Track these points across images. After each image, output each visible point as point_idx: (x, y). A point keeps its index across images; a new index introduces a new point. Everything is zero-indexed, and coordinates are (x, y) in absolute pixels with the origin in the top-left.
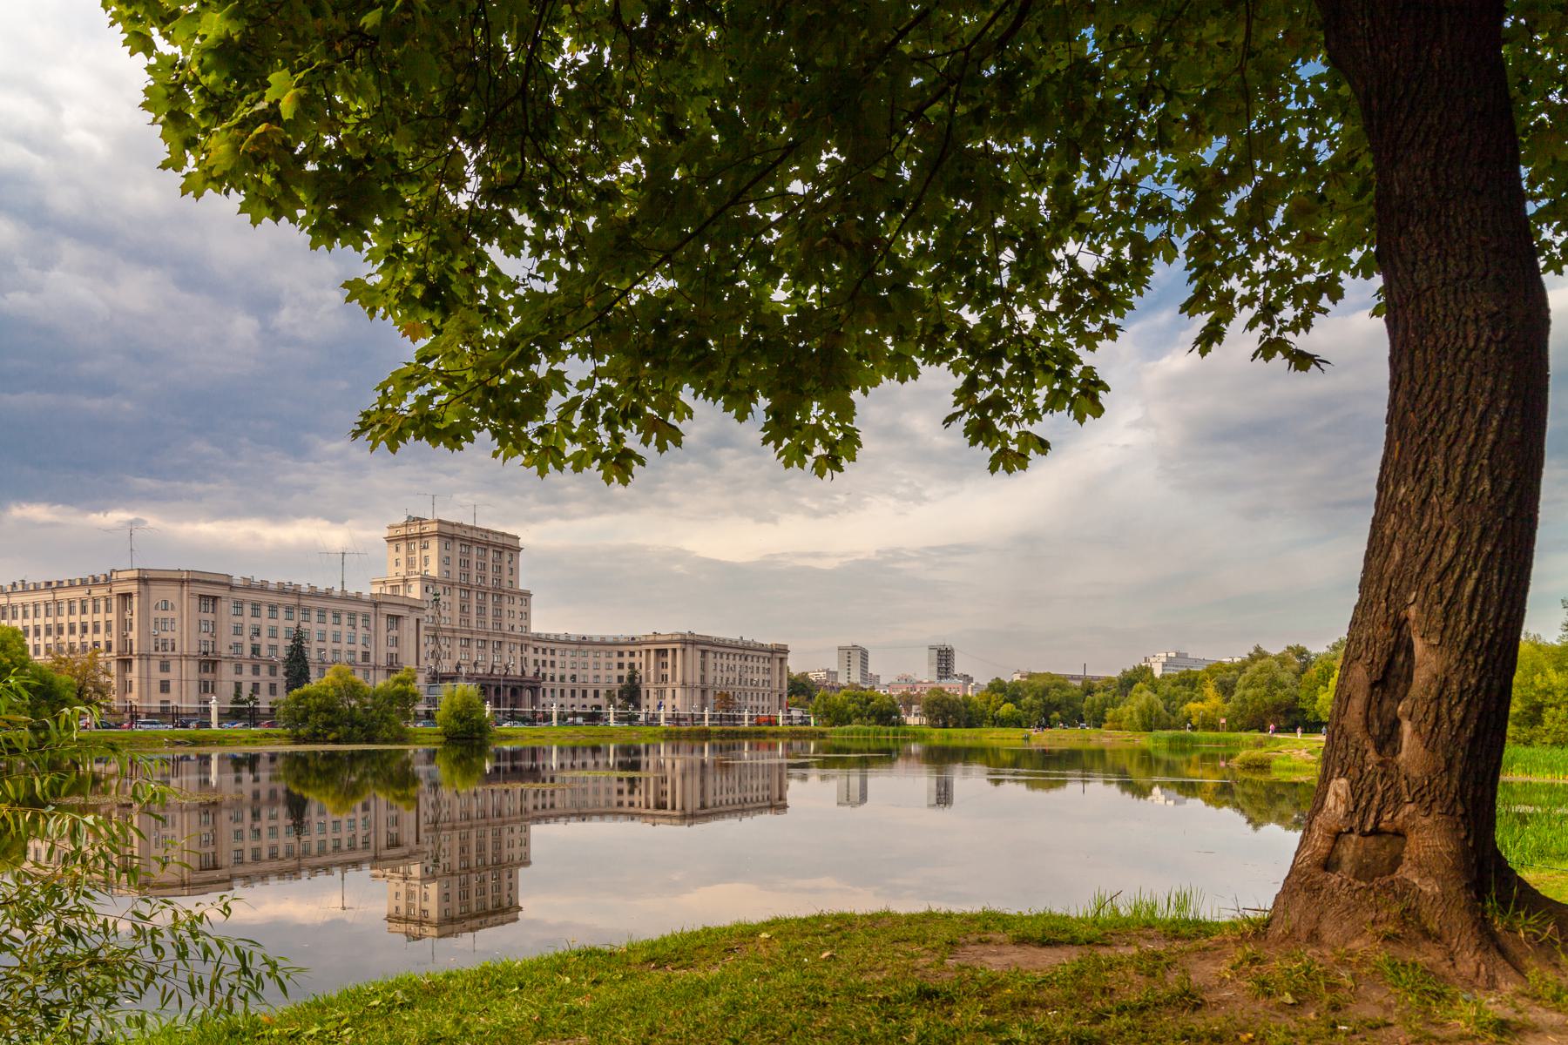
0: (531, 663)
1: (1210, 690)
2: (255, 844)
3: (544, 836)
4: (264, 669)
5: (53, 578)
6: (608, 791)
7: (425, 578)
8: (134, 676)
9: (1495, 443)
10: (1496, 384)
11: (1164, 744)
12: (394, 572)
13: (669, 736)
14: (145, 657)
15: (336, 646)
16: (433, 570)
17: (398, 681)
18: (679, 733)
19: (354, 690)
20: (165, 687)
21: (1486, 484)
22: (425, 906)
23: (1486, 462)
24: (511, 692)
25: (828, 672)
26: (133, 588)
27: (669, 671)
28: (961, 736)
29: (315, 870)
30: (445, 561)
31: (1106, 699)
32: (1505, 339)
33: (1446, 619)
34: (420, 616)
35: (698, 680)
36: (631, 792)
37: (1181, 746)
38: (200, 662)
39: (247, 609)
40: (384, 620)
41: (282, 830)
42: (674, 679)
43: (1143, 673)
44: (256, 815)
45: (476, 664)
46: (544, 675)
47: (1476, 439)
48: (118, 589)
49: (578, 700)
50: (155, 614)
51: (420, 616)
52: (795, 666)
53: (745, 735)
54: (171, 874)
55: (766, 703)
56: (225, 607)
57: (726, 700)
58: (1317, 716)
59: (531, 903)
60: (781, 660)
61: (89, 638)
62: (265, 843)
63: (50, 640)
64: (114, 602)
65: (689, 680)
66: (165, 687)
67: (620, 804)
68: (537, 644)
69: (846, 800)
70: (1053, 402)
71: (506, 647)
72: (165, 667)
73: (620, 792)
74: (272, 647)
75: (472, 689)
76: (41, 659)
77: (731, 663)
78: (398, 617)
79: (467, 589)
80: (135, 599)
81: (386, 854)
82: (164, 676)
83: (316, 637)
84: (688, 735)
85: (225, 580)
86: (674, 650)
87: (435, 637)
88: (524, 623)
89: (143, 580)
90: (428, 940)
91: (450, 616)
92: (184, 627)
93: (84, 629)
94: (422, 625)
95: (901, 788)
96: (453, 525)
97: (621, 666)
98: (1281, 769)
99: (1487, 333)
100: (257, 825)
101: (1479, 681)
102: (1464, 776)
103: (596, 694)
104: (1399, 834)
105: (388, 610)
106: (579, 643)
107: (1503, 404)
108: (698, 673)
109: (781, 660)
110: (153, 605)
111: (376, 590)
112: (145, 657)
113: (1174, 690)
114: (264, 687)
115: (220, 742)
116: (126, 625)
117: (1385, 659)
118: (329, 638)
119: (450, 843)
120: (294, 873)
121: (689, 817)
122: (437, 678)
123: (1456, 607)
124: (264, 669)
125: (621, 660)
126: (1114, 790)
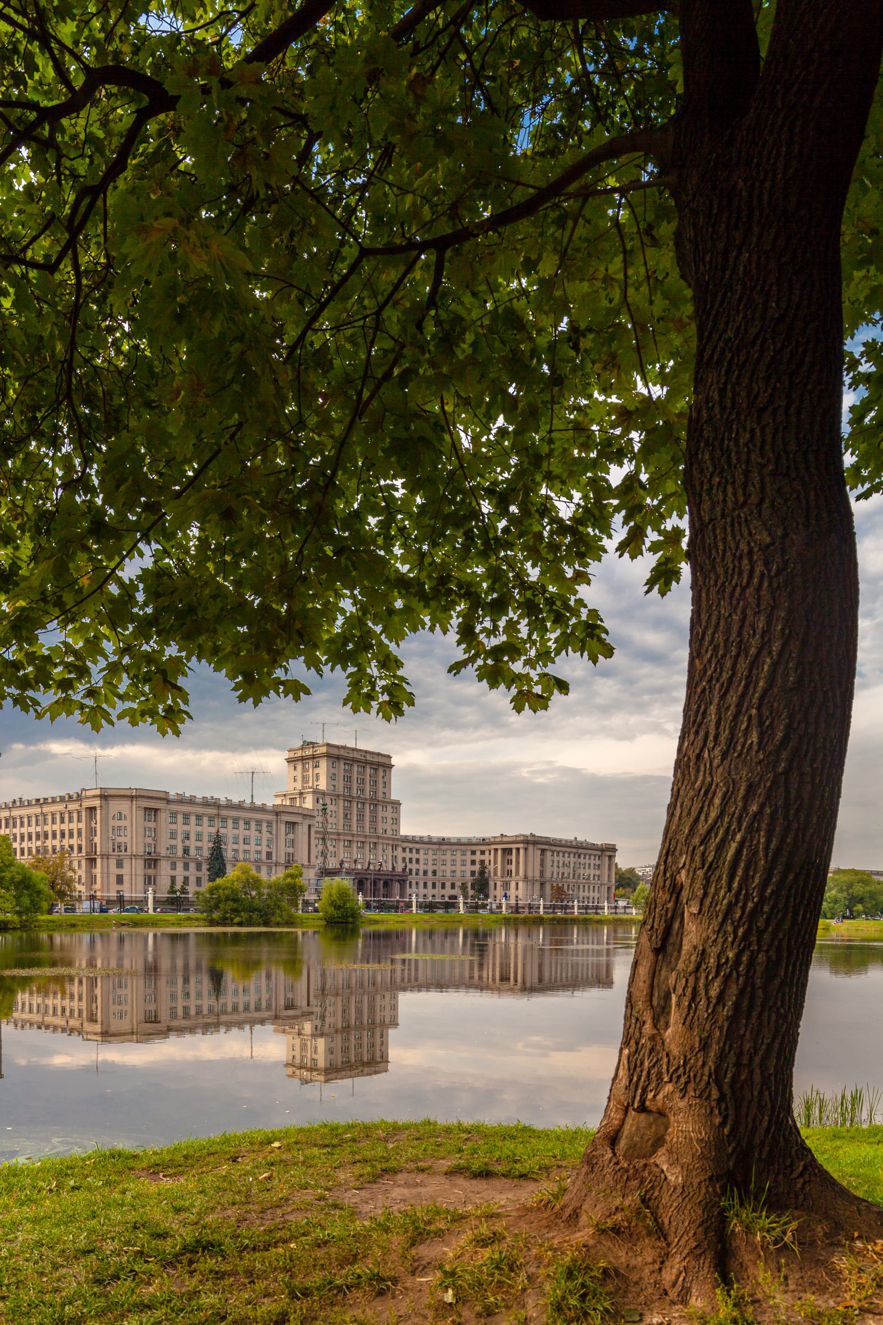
0: (400, 860)
3: (409, 1002)
4: (192, 866)
5: (41, 796)
8: (98, 871)
9: (765, 691)
10: (769, 623)
12: (292, 787)
13: (507, 921)
14: (106, 856)
15: (247, 847)
16: (323, 785)
18: (516, 919)
19: (256, 883)
20: (120, 880)
21: (754, 737)
23: (754, 712)
24: (382, 885)
26: (97, 803)
29: (229, 1026)
30: (332, 777)
32: (779, 572)
33: (706, 887)
34: (311, 822)
35: (537, 874)
38: (145, 860)
39: (180, 818)
40: (283, 827)
41: (205, 993)
42: (517, 873)
44: (186, 980)
45: (355, 861)
46: (411, 870)
47: (746, 687)
48: (87, 804)
49: (438, 891)
50: (112, 823)
51: (311, 822)
52: (623, 862)
53: (574, 921)
54: (123, 1025)
55: (596, 895)
56: (163, 816)
57: (559, 893)
59: (402, 1054)
60: (610, 857)
61: (66, 842)
62: (193, 1003)
63: (39, 843)
64: (84, 813)
65: (530, 874)
66: (120, 880)
70: (564, 643)
71: (380, 847)
72: (120, 865)
74: (198, 849)
75: (346, 882)
76: (24, 860)
78: (294, 824)
79: (349, 799)
80: (98, 812)
81: (284, 1015)
82: (119, 872)
83: (231, 840)
84: (525, 921)
85: (163, 796)
86: (518, 849)
87: (323, 839)
89: (104, 797)
91: (335, 823)
92: (133, 834)
93: (63, 835)
94: (313, 830)
96: (338, 747)
97: (473, 862)
99: (759, 569)
101: (738, 956)
102: (722, 1057)
103: (453, 886)
104: (661, 1113)
105: (285, 817)
107: (776, 646)
108: (538, 868)
110: (111, 816)
111: (278, 802)
112: (106, 856)
114: (192, 880)
115: (154, 924)
116: (92, 832)
117: (663, 925)
121: (528, 989)
122: (326, 872)
123: (718, 872)
124: (192, 866)
125: (473, 858)
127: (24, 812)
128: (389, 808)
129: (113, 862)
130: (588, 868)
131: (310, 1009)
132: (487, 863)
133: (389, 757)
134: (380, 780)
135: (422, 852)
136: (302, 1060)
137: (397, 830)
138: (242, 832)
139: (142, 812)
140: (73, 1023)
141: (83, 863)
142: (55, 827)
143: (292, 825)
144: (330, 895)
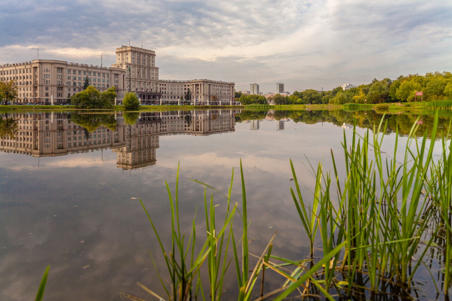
1: (361, 92)
2: (75, 142)
3: (162, 139)
5: (15, 63)
6: (182, 127)
7: (127, 64)
8: (38, 92)
11: (347, 107)
12: (118, 62)
14: (41, 86)
15: (99, 83)
16: (129, 61)
17: (109, 91)
22: (128, 160)
24: (150, 97)
25: (248, 92)
26: (37, 65)
27: (199, 91)
28: (285, 107)
29: (92, 149)
30: (133, 59)
31: (329, 97)
34: (124, 74)
35: (208, 93)
36: (189, 126)
37: (353, 107)
39: (72, 72)
40: (113, 76)
41: (83, 138)
42: (201, 93)
43: (340, 89)
44: (75, 133)
46: (163, 92)
52: (237, 89)
54: (49, 150)
56: (65, 71)
58: (396, 98)
60: (233, 87)
62: (78, 141)
64: (32, 69)
65: (205, 93)
67: (186, 129)
68: (160, 83)
69: (253, 128)
72: (47, 89)
73: (185, 126)
74: (79, 83)
77: (218, 88)
78: (118, 74)
80: (38, 69)
81: (115, 144)
82: (47, 91)
83: (93, 80)
85: (65, 63)
86: (201, 84)
88: (157, 77)
89: (41, 63)
90: (129, 170)
93: (24, 78)
94: (125, 77)
95: (269, 124)
96: (135, 48)
97: (185, 89)
98: (392, 109)
100: (75, 136)
105: (115, 72)
106: (173, 83)
109: (233, 87)
112: (41, 86)
113: (349, 94)
118: (97, 80)
119: (134, 141)
120: (87, 150)
121: (206, 133)
125: (185, 87)
126: (331, 124)
127: (8, 69)
128: (155, 70)
129: (44, 88)
130: (225, 91)
131: (124, 142)
132: (190, 89)
133: (154, 52)
134: (151, 60)
135: (167, 85)
136: (123, 161)
137: (157, 78)
138: (97, 77)
139: (56, 69)
140: (28, 150)
141: (32, 88)
142: (21, 75)
143: (117, 75)
144: (127, 98)
